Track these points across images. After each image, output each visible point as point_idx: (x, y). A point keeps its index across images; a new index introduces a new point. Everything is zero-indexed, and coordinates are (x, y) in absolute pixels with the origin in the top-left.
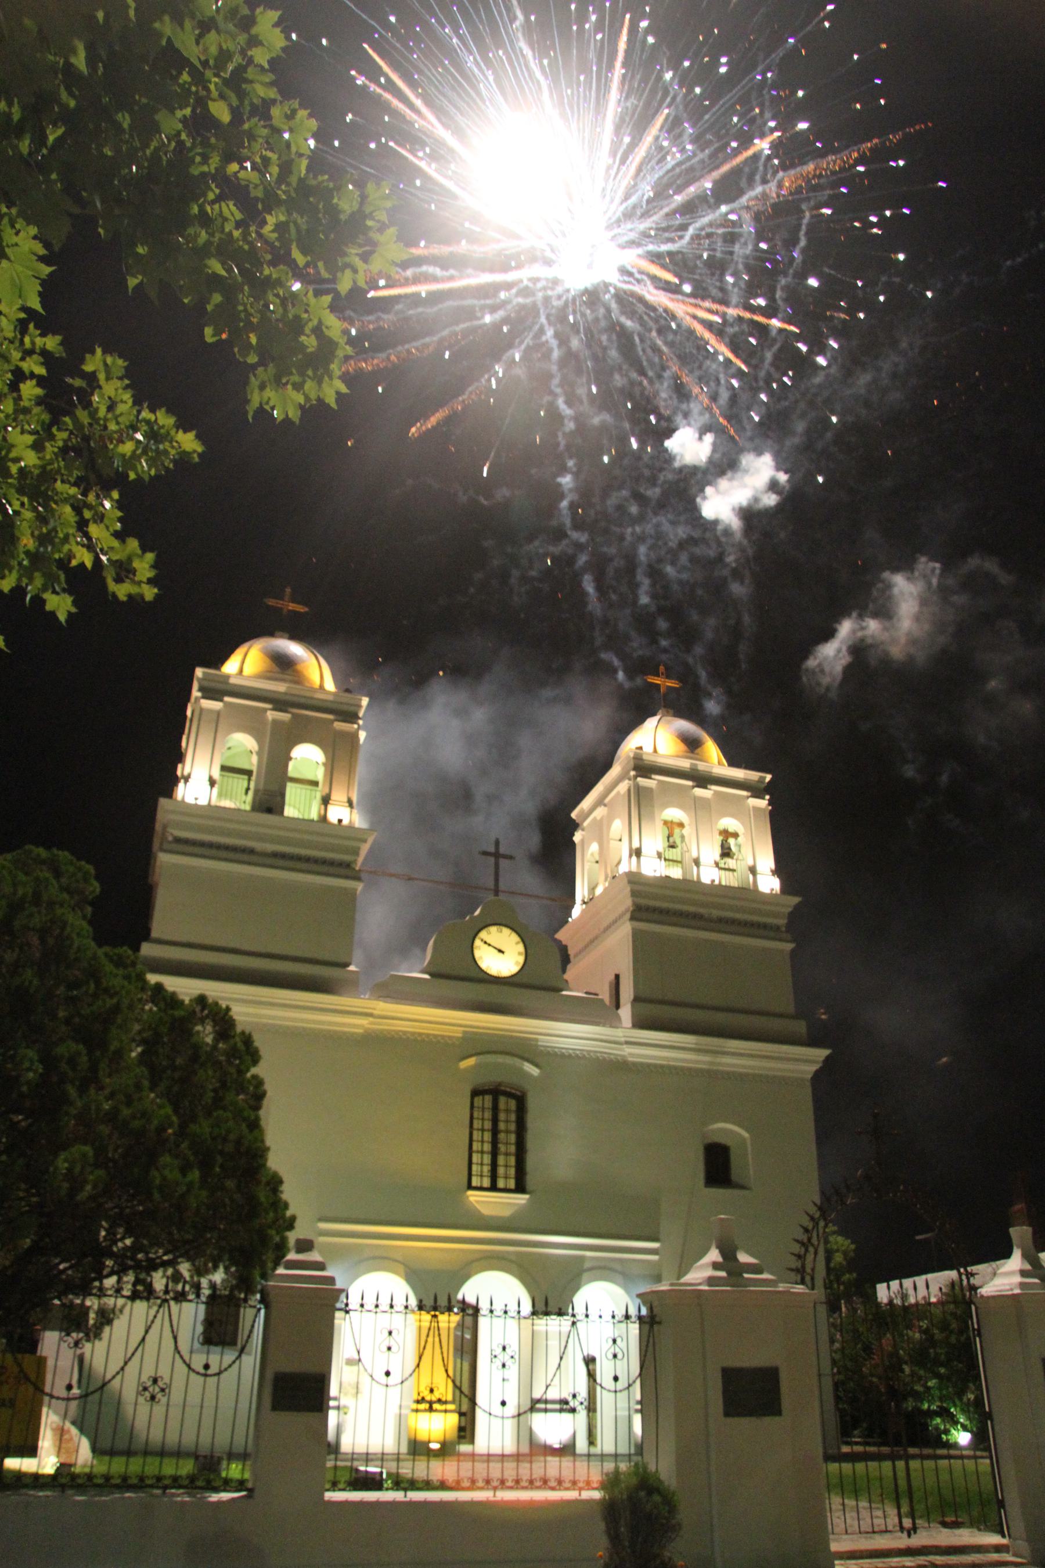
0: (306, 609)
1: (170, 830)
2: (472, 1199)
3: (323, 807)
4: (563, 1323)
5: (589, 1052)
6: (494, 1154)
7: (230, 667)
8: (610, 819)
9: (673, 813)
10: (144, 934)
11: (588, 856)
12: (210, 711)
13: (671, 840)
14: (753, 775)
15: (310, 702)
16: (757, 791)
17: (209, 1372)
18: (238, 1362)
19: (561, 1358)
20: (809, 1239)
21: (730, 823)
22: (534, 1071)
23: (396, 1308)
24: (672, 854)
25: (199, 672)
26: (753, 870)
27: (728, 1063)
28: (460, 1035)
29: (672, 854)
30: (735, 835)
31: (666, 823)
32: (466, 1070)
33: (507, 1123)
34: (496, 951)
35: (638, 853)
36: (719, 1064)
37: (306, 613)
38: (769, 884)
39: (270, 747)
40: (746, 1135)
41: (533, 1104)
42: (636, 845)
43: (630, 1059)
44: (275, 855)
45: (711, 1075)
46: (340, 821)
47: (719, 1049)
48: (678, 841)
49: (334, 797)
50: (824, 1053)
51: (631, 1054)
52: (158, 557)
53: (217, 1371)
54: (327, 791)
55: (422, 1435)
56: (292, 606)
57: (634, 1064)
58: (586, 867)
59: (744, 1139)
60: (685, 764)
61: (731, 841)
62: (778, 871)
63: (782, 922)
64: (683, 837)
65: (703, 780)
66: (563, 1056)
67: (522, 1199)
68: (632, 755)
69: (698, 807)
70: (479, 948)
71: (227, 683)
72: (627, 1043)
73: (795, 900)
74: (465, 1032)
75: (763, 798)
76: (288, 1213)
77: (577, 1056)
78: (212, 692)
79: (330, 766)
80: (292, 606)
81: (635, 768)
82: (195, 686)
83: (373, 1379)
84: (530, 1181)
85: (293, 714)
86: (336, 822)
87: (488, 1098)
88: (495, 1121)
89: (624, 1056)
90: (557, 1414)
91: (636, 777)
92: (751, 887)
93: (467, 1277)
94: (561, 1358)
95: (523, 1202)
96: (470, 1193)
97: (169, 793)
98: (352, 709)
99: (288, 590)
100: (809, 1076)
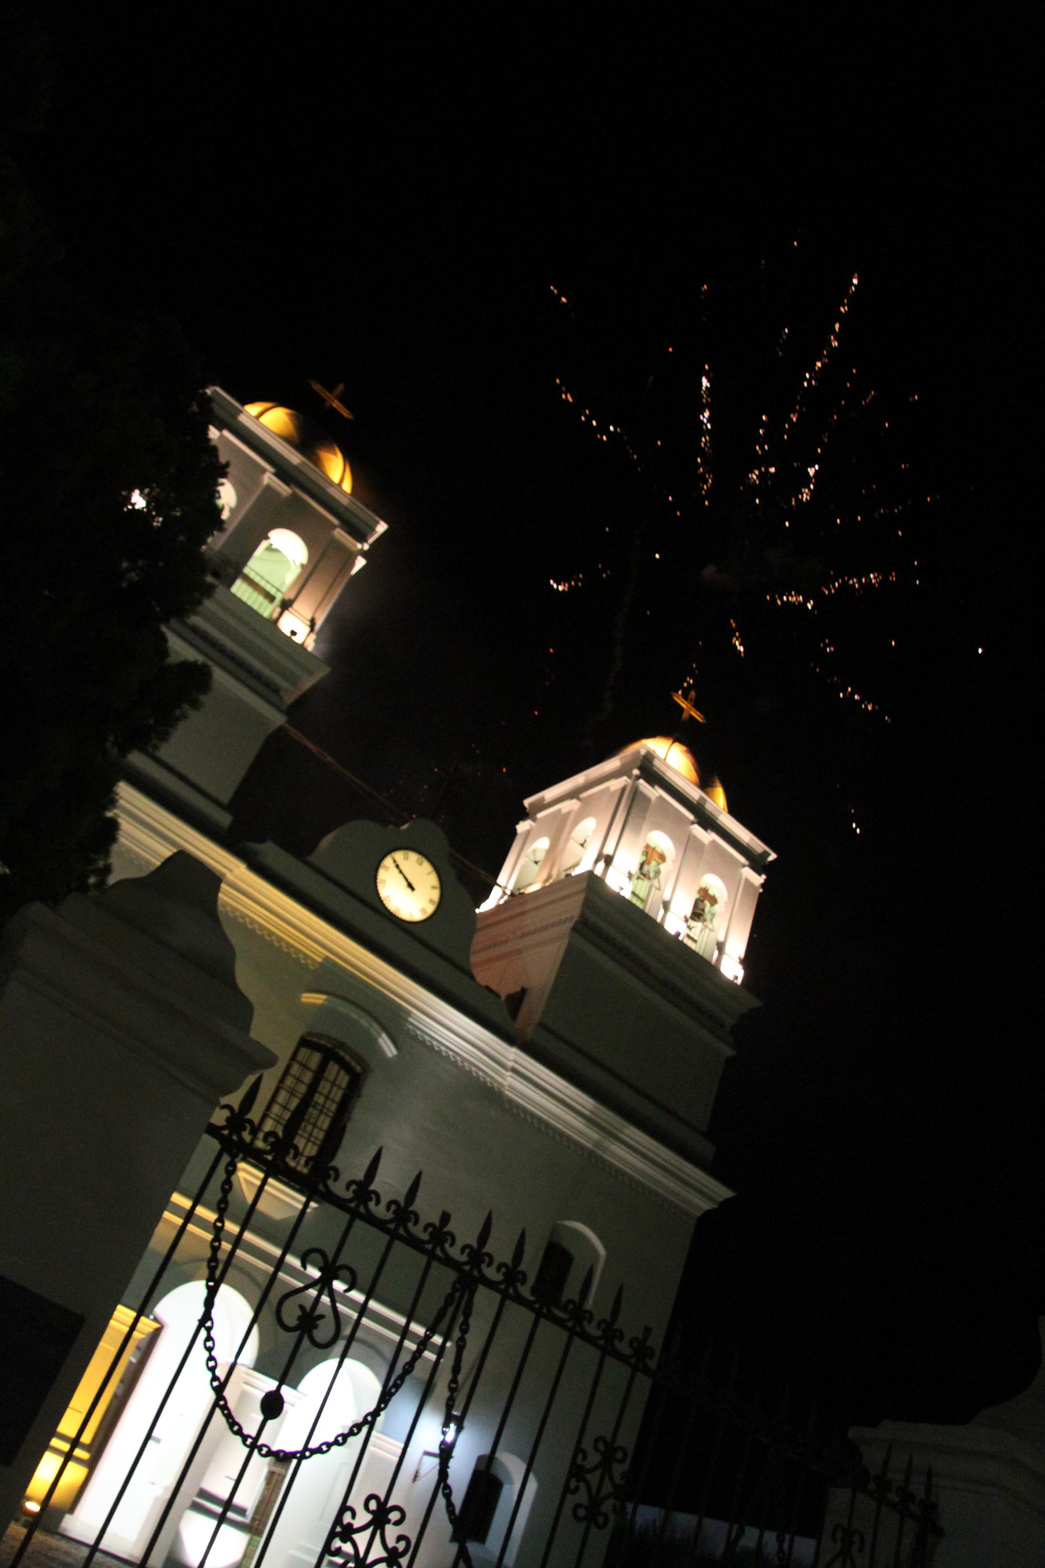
0: (350, 417)
3: (278, 610)
8: (580, 817)
9: (660, 840)
11: (529, 850)
14: (758, 845)
16: (756, 863)
21: (715, 884)
22: (390, 1050)
26: (721, 947)
27: (618, 1154)
28: (319, 960)
31: (648, 846)
34: (405, 884)
35: (609, 860)
36: (606, 1150)
37: (347, 420)
38: (732, 969)
40: (602, 1251)
41: (371, 1088)
42: (608, 850)
43: (507, 1093)
47: (614, 1131)
49: (296, 606)
50: (724, 1193)
51: (512, 1088)
54: (291, 596)
56: (336, 404)
57: (511, 1101)
58: (521, 862)
60: (695, 793)
62: (746, 962)
63: (730, 1021)
64: (658, 873)
65: (707, 822)
66: (431, 1048)
69: (689, 846)
70: (387, 868)
72: (514, 1070)
73: (756, 1003)
77: (448, 1057)
79: (309, 570)
80: (336, 404)
81: (640, 768)
87: (316, 1058)
89: (503, 1086)
91: (638, 778)
98: (361, 526)
99: (341, 387)
100: (698, 1214)
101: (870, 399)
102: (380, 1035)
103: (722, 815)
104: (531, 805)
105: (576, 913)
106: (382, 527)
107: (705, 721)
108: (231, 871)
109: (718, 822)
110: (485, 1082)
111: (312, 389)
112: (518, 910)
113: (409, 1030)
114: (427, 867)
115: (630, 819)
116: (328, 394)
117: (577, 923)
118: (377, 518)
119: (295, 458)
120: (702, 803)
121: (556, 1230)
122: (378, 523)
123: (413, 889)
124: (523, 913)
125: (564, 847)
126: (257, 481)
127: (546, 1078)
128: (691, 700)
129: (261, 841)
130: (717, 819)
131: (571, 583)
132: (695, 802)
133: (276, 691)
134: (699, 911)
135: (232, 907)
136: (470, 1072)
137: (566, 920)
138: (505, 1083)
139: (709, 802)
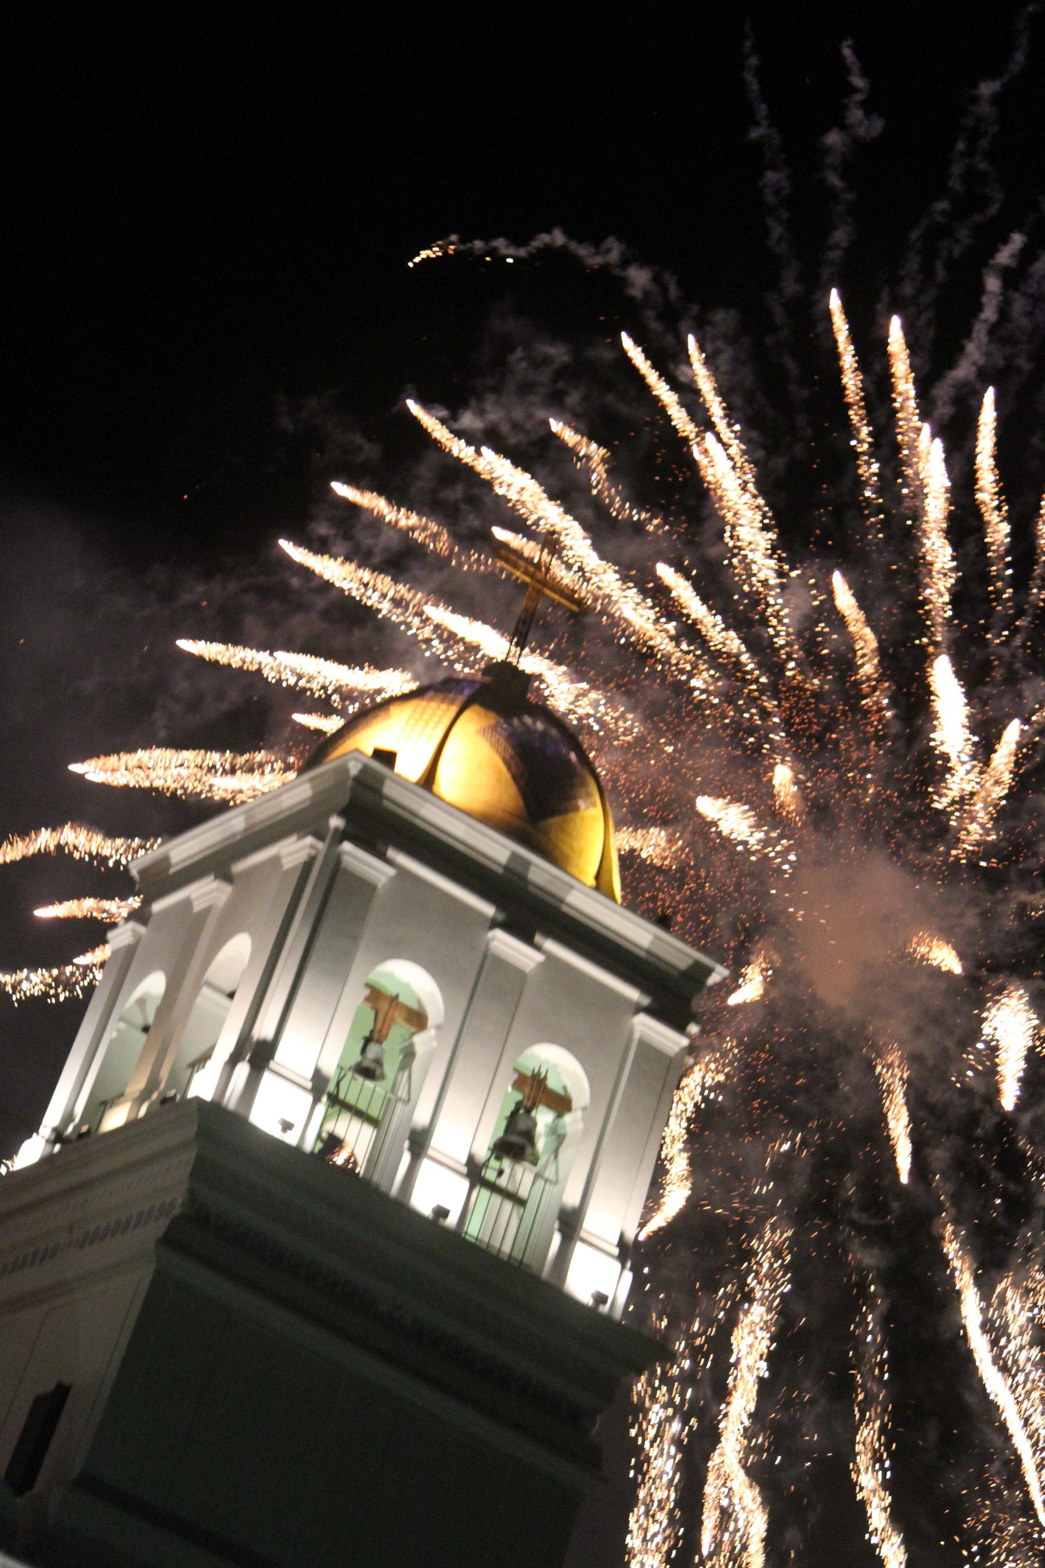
4: (623, 835)
13: (373, 1050)
24: (357, 1090)
29: (357, 1090)
30: (561, 1104)
31: (375, 995)
42: (264, 1029)
48: (390, 1068)
52: (957, 565)
58: (110, 1034)
61: (543, 1117)
64: (409, 1054)
68: (354, 769)
81: (343, 813)
91: (342, 836)
92: (545, 1273)
103: (574, 892)
105: (179, 1196)
109: (565, 908)
115: (319, 943)
117: (175, 1224)
120: (518, 868)
124: (86, 1185)
125: (191, 1002)
130: (562, 901)
132: (500, 871)
134: (515, 1139)
139: (536, 866)
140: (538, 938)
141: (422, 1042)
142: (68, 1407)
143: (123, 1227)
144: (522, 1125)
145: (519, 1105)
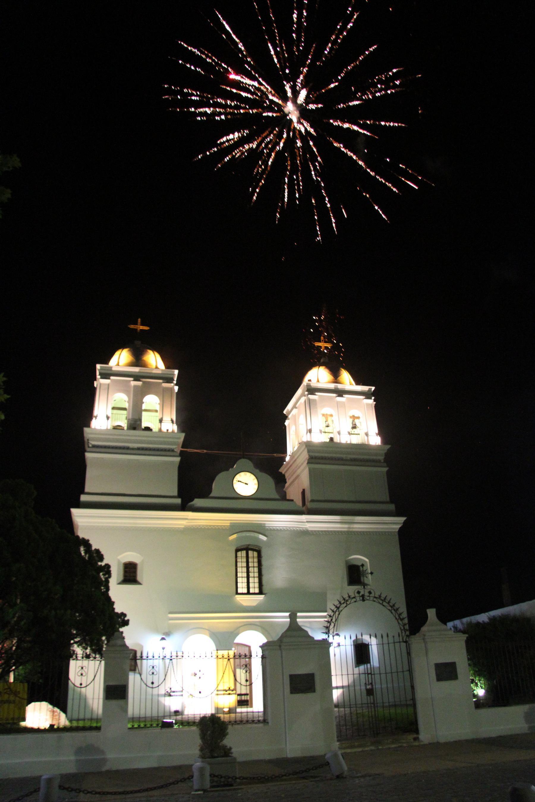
0: (148, 328)
1: (90, 442)
2: (238, 599)
3: (160, 424)
5: (290, 527)
6: (248, 577)
7: (113, 362)
9: (327, 410)
10: (82, 491)
12: (105, 384)
14: (365, 388)
15: (151, 375)
16: (367, 395)
17: (82, 686)
18: (93, 682)
19: (224, 673)
20: (332, 620)
22: (264, 538)
23: (155, 658)
25: (98, 366)
27: (357, 527)
28: (229, 525)
29: (327, 429)
30: (358, 418)
31: (323, 415)
32: (232, 540)
33: (253, 563)
34: (244, 484)
35: (310, 431)
36: (353, 528)
38: (375, 440)
39: (133, 399)
40: (367, 560)
42: (309, 428)
43: (309, 529)
44: (139, 449)
45: (349, 534)
46: (168, 430)
48: (330, 424)
49: (164, 419)
50: (402, 519)
53: (85, 686)
54: (161, 416)
55: (220, 706)
56: (142, 327)
57: (312, 531)
58: (291, 438)
59: (366, 562)
60: (332, 386)
61: (357, 421)
63: (382, 458)
65: (340, 393)
67: (261, 597)
71: (111, 370)
72: (307, 522)
74: (231, 523)
75: (371, 399)
76: (126, 619)
77: (284, 529)
78: (106, 375)
80: (142, 327)
81: (307, 391)
82: (98, 373)
83: (147, 686)
84: (265, 589)
85: (144, 382)
86: (166, 431)
87: (244, 553)
88: (248, 562)
89: (307, 528)
90: (223, 696)
93: (238, 634)
94: (224, 673)
95: (262, 598)
96: (237, 596)
97: (88, 426)
99: (139, 320)
100: (397, 530)
101: (343, 149)
102: (259, 536)
104: (286, 412)
105: (307, 456)
106: (176, 372)
107: (332, 345)
108: (188, 516)
109: (346, 390)
110: (301, 530)
111: (131, 328)
112: (294, 460)
113: (267, 529)
114: (248, 474)
116: (137, 326)
118: (173, 370)
119: (136, 370)
121: (347, 562)
122: (174, 371)
123: (247, 484)
124: (295, 460)
126: (129, 386)
127: (321, 518)
128: (323, 341)
129: (192, 500)
131: (378, 89)
133: (173, 450)
135: (195, 525)
136: (294, 530)
137: (304, 461)
138: (307, 527)
140: (344, 396)
141: (333, 418)
142: (305, 491)
143: (302, 464)
144: (354, 424)
145: (353, 421)
